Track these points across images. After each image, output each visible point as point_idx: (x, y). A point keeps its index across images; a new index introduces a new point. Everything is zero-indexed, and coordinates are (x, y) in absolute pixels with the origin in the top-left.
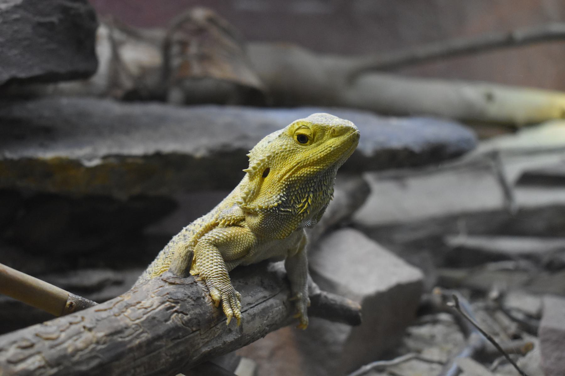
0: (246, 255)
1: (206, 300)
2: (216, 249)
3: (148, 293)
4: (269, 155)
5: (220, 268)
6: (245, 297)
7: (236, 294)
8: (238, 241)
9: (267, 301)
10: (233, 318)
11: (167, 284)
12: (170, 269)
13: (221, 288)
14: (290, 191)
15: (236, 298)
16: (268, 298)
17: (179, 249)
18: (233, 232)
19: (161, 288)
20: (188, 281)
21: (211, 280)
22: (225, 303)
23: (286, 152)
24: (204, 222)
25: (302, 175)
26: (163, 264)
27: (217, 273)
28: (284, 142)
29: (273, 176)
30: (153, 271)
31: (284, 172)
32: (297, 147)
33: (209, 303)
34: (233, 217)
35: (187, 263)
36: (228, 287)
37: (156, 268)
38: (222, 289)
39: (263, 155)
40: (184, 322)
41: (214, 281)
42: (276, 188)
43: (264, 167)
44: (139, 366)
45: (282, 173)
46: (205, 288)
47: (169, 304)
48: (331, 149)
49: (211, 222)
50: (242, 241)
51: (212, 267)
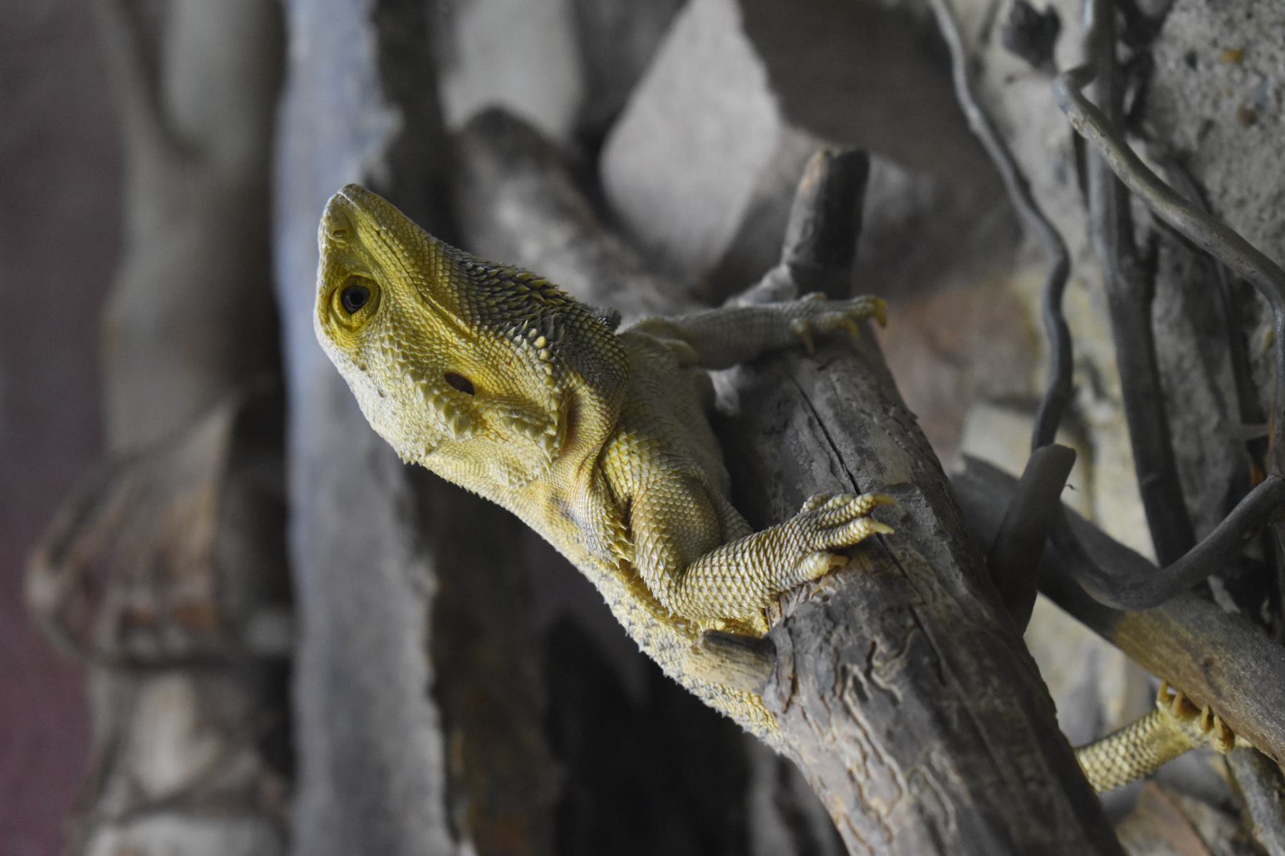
0: (701, 485)
1: (831, 590)
2: (694, 569)
3: (823, 749)
4: (408, 378)
5: (743, 557)
6: (814, 479)
7: (811, 509)
8: (666, 510)
9: (822, 417)
10: (872, 514)
11: (796, 699)
12: (755, 690)
13: (796, 551)
15: (821, 509)
16: (811, 414)
17: (701, 671)
18: (644, 524)
19: (808, 715)
20: (785, 641)
21: (776, 579)
22: (836, 539)
23: (398, 335)
24: (622, 599)
25: (456, 287)
26: (741, 701)
27: (757, 564)
29: (466, 360)
30: (761, 724)
32: (386, 312)
33: (837, 584)
34: (607, 523)
35: (738, 649)
36: (793, 532)
37: (753, 716)
38: (800, 548)
40: (894, 652)
41: (779, 571)
42: (494, 349)
44: (1018, 770)
45: (454, 334)
46: (798, 593)
47: (850, 695)
48: (384, 230)
49: (622, 582)
50: (668, 499)
51: (743, 578)
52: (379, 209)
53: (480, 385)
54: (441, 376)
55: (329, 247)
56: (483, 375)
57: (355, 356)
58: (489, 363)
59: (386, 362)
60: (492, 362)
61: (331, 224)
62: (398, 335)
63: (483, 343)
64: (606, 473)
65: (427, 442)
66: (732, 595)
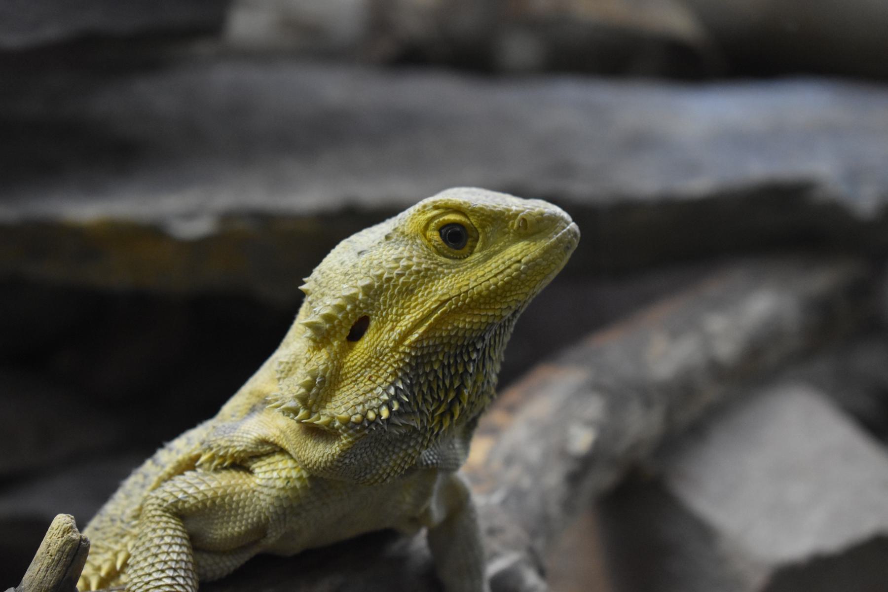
4: (367, 281)
5: (168, 577)
14: (418, 373)
23: (411, 275)
25: (453, 334)
28: (402, 250)
31: (409, 325)
32: (437, 264)
34: (231, 450)
35: (59, 572)
39: (350, 283)
43: (355, 315)
45: (404, 328)
48: (520, 267)
51: (150, 574)
52: (544, 263)
53: (354, 349)
54: (365, 313)
55: (511, 213)
56: (363, 353)
57: (401, 230)
58: (373, 360)
59: (387, 261)
60: (374, 363)
61: (534, 216)
62: (411, 275)
63: (393, 356)
64: (276, 453)
65: (313, 292)
66: (140, 561)
